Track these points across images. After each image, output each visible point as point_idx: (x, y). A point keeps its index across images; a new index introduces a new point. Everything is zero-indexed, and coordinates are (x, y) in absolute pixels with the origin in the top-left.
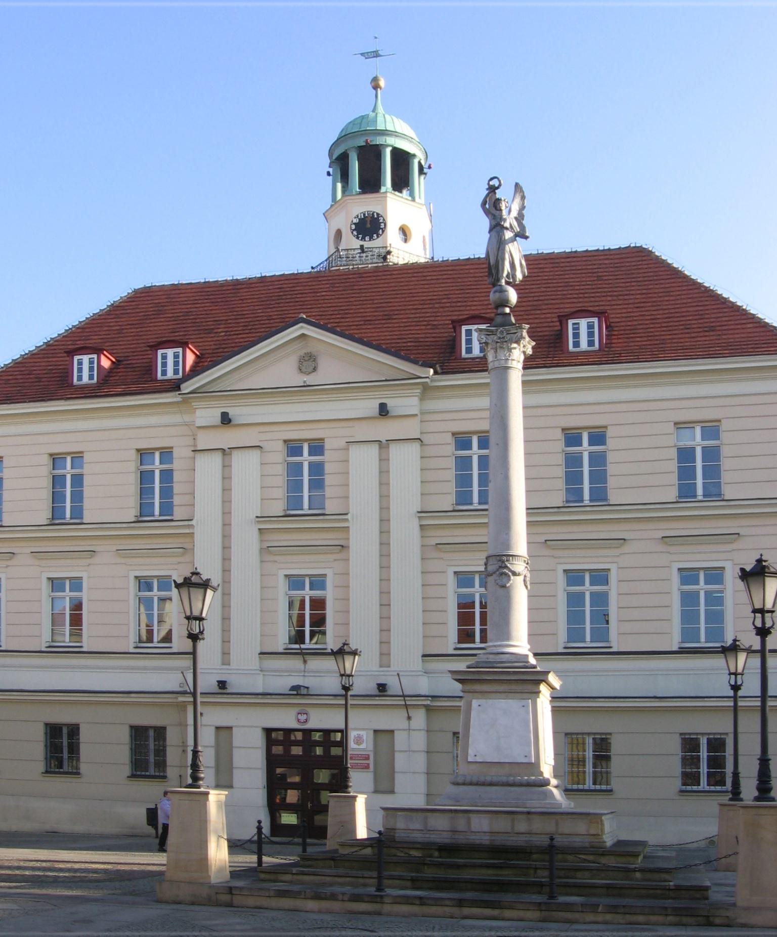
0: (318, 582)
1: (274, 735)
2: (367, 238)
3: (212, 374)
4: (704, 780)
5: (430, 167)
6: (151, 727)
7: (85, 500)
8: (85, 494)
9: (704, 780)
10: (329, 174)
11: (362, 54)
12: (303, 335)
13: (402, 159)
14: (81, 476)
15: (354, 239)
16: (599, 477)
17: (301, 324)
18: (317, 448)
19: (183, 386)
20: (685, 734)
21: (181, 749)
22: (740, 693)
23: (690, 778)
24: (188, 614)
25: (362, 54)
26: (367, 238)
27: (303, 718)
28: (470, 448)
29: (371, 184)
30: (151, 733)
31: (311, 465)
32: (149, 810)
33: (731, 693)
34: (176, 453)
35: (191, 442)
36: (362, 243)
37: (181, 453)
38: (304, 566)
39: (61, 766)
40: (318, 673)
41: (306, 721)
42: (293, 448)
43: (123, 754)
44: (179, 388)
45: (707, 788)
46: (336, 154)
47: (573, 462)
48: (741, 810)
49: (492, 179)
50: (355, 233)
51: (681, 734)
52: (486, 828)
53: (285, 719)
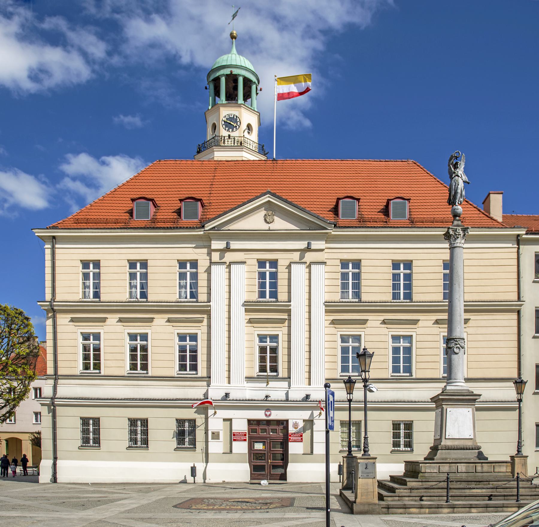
0: (274, 338)
1: (252, 422)
2: (231, 130)
5: (261, 90)
6: (91, 418)
8: (149, 284)
12: (269, 201)
13: (247, 83)
15: (224, 130)
16: (408, 287)
17: (268, 195)
18: (274, 263)
20: (395, 421)
23: (396, 444)
24: (466, 377)
26: (231, 130)
27: (268, 413)
29: (231, 97)
32: (192, 467)
34: (200, 263)
36: (228, 133)
38: (268, 330)
39: (136, 443)
40: (275, 389)
41: (270, 415)
42: (261, 263)
43: (78, 435)
44: (203, 227)
45: (404, 449)
47: (396, 277)
49: (451, 159)
50: (224, 126)
51: (393, 421)
52: (464, 470)
53: (260, 415)
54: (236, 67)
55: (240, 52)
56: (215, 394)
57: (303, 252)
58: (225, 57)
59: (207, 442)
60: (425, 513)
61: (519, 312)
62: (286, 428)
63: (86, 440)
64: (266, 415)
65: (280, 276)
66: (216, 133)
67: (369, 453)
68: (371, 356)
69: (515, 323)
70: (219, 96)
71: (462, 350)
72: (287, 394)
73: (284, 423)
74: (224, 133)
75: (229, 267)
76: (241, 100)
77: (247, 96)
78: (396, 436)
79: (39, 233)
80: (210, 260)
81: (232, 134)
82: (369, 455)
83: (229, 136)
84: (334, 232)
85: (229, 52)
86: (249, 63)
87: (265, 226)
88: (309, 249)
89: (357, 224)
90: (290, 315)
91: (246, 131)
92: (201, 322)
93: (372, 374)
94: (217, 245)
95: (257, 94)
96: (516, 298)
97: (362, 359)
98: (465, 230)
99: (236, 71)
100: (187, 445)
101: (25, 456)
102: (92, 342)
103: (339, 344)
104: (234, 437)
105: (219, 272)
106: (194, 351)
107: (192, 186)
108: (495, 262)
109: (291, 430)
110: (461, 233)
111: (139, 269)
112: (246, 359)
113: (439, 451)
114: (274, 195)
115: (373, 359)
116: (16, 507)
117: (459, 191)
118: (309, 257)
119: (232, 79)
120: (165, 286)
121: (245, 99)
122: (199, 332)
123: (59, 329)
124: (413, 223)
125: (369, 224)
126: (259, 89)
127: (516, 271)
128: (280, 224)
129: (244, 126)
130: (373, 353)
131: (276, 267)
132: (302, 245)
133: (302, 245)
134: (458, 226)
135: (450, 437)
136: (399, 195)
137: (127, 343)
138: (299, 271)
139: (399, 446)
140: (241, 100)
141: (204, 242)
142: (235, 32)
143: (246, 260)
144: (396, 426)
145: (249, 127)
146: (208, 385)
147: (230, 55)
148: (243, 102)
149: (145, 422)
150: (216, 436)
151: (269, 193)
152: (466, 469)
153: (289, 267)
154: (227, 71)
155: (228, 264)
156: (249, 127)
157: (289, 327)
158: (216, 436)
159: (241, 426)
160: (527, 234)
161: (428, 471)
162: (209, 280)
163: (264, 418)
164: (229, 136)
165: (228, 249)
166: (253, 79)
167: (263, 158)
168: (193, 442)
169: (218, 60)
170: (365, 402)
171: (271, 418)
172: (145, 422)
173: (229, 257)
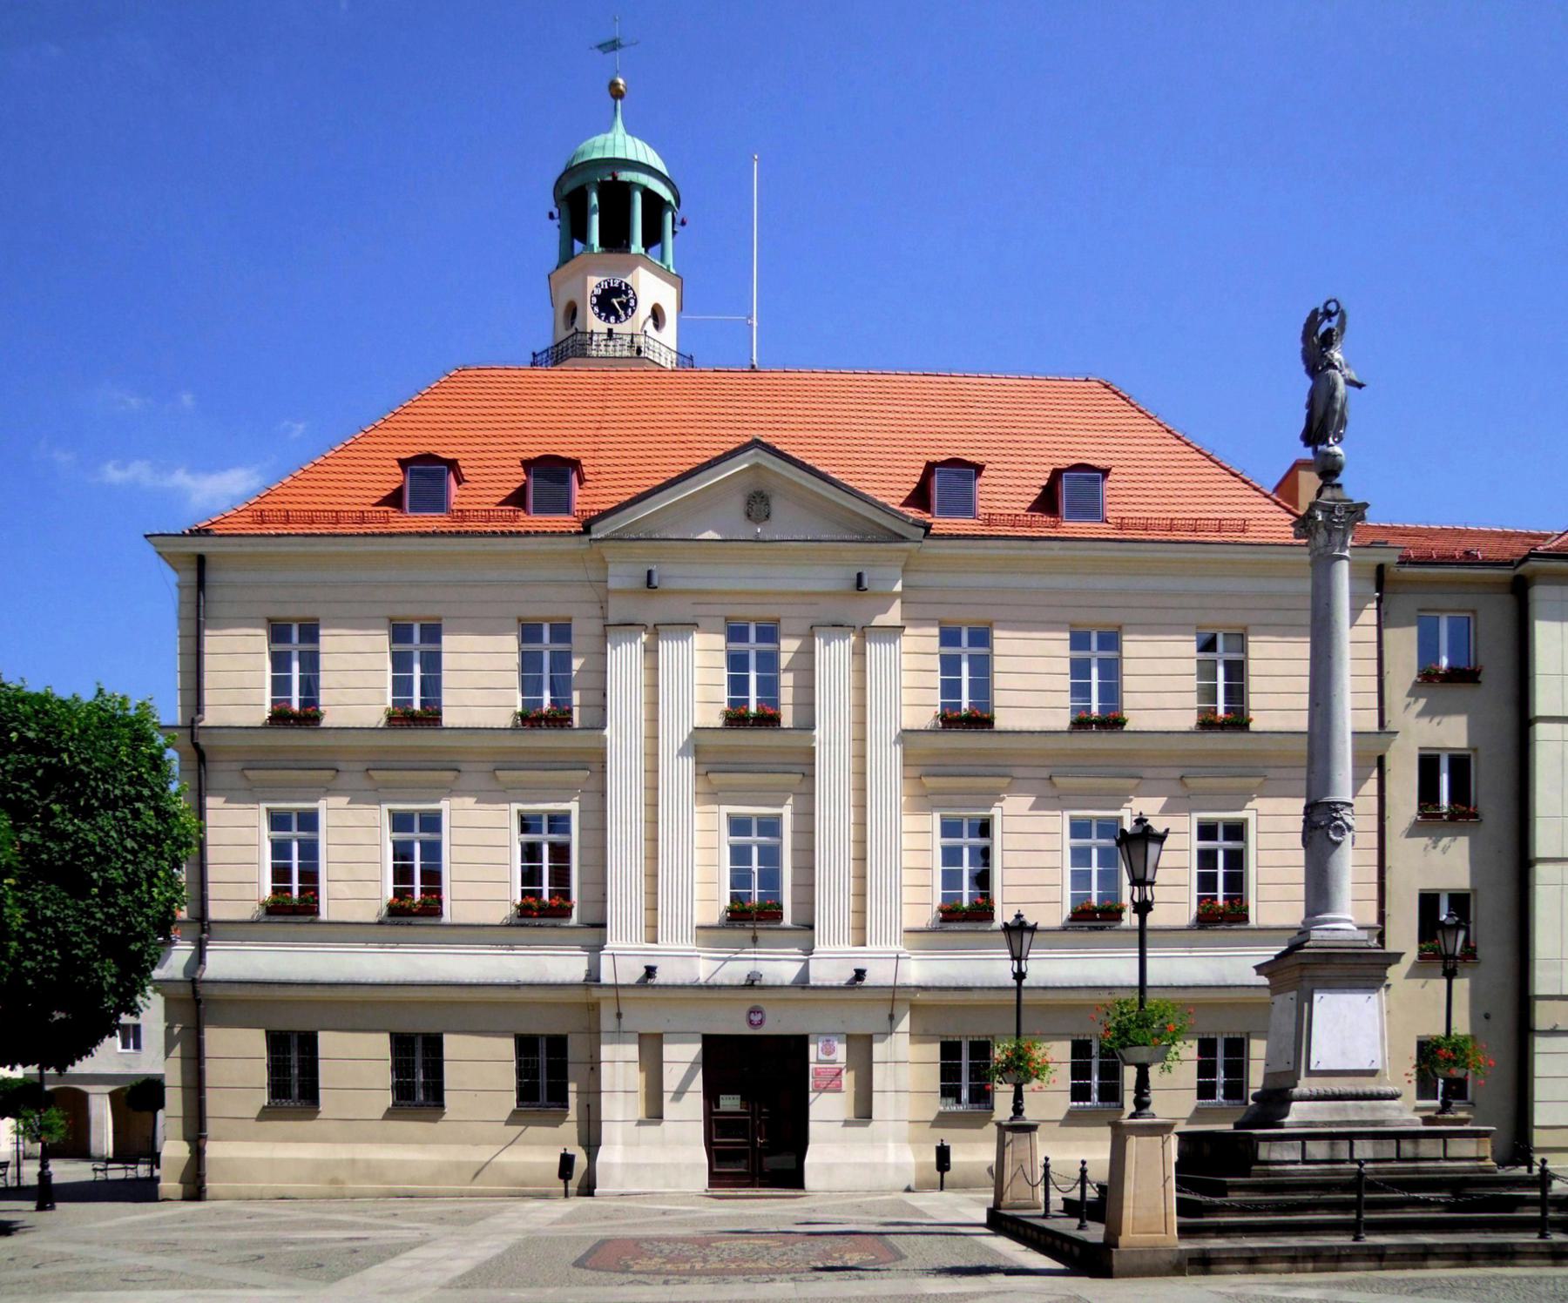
2: (612, 319)
3: (635, 514)
4: (1220, 1092)
5: (683, 223)
7: (444, 692)
9: (1220, 1092)
10: (551, 216)
11: (600, 47)
13: (654, 205)
14: (438, 654)
19: (594, 528)
21: (588, 1067)
22: (1025, 983)
25: (600, 47)
26: (612, 319)
28: (959, 644)
29: (615, 239)
30: (419, 1045)
31: (759, 654)
33: (1014, 983)
35: (596, 611)
37: (585, 629)
41: (761, 1022)
46: (569, 187)
48: (603, 1156)
52: (1369, 1154)
53: (734, 1024)
55: (630, 131)
58: (599, 140)
60: (1305, 1271)
64: (751, 1022)
66: (577, 324)
67: (1152, 1109)
68: (1160, 839)
70: (583, 236)
71: (1349, 835)
74: (596, 324)
76: (637, 247)
77: (653, 236)
80: (605, 618)
81: (617, 328)
82: (1153, 1116)
83: (610, 332)
85: (608, 127)
91: (651, 321)
95: (674, 233)
97: (1137, 851)
99: (625, 176)
101: (1260, 969)
106: (561, 853)
107: (550, 432)
112: (703, 881)
113: (1294, 1105)
115: (1166, 844)
116: (135, 1277)
119: (616, 196)
120: (482, 681)
121: (647, 244)
126: (678, 220)
127: (1375, 655)
129: (644, 310)
130: (1167, 831)
135: (1322, 1067)
140: (637, 247)
142: (621, 81)
143: (697, 620)
145: (657, 315)
147: (610, 136)
148: (642, 251)
152: (1375, 1152)
155: (651, 626)
156: (657, 315)
161: (1275, 1156)
164: (610, 332)
166: (667, 195)
169: (585, 145)
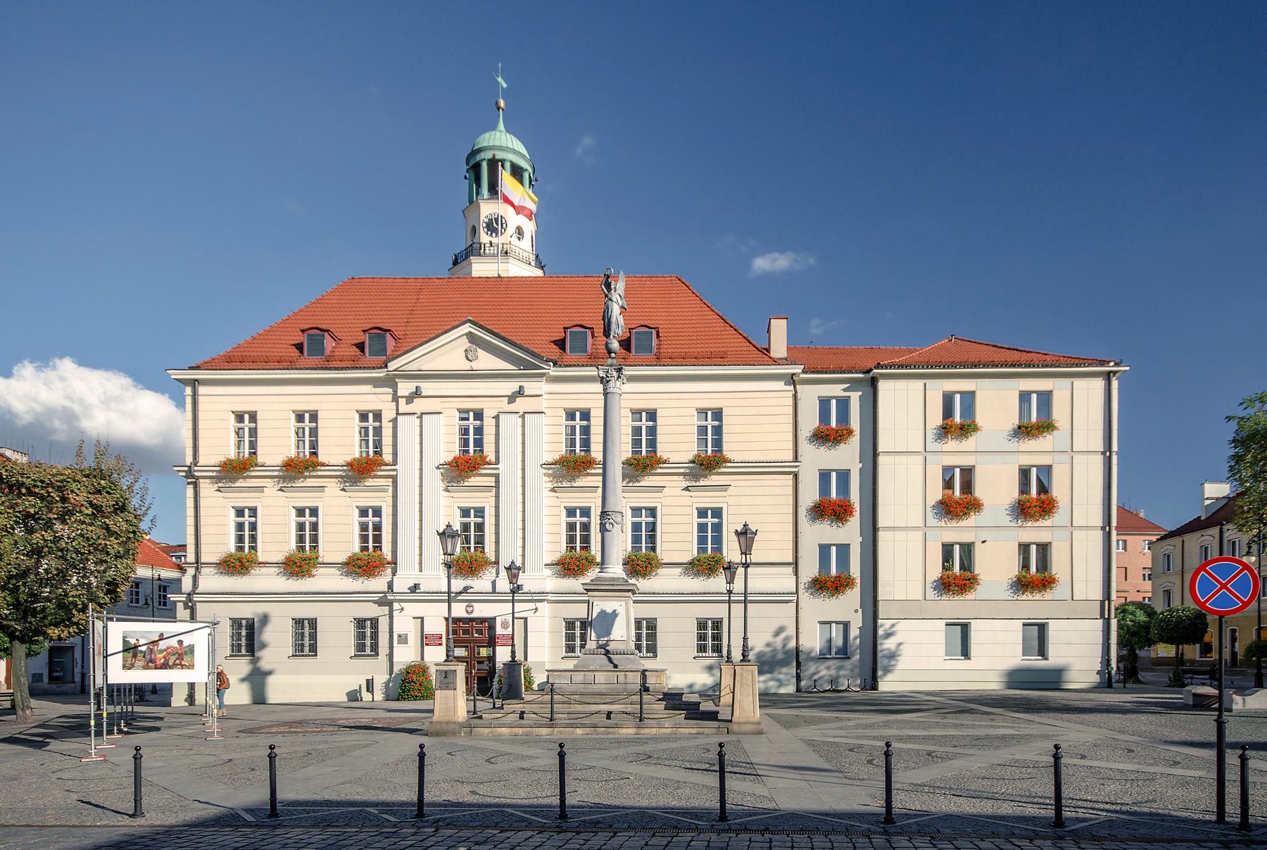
18: (479, 415)
39: (240, 651)
42: (464, 413)
54: (501, 148)
55: (509, 130)
56: (401, 584)
57: (512, 399)
59: (391, 647)
61: (796, 476)
62: (492, 628)
63: (360, 647)
65: (593, 430)
69: (790, 491)
72: (494, 583)
73: (491, 622)
75: (421, 417)
78: (702, 637)
79: (176, 374)
81: (494, 240)
84: (553, 371)
85: (493, 127)
86: (520, 144)
87: (466, 365)
88: (520, 393)
89: (585, 361)
90: (497, 482)
92: (386, 491)
93: (755, 556)
94: (405, 388)
96: (791, 458)
98: (619, 370)
99: (499, 155)
100: (368, 651)
102: (308, 519)
103: (564, 519)
104: (426, 640)
105: (408, 427)
108: (763, 411)
109: (499, 630)
110: (615, 374)
111: (308, 419)
114: (474, 323)
117: (613, 320)
118: (521, 404)
122: (593, 506)
123: (203, 503)
124: (659, 360)
125: (335, 364)
128: (486, 361)
131: (589, 420)
132: (510, 387)
133: (510, 387)
134: (611, 365)
136: (646, 323)
137: (293, 519)
138: (510, 425)
139: (573, 651)
141: (390, 382)
144: (702, 625)
146: (394, 573)
149: (313, 623)
150: (403, 639)
151: (470, 321)
153: (497, 418)
154: (488, 155)
156: (520, 232)
157: (497, 497)
158: (403, 639)
159: (436, 626)
160: (804, 372)
162: (395, 436)
163: (465, 615)
165: (417, 394)
167: (539, 273)
168: (375, 648)
170: (745, 594)
171: (474, 615)
172: (313, 623)
173: (419, 405)
